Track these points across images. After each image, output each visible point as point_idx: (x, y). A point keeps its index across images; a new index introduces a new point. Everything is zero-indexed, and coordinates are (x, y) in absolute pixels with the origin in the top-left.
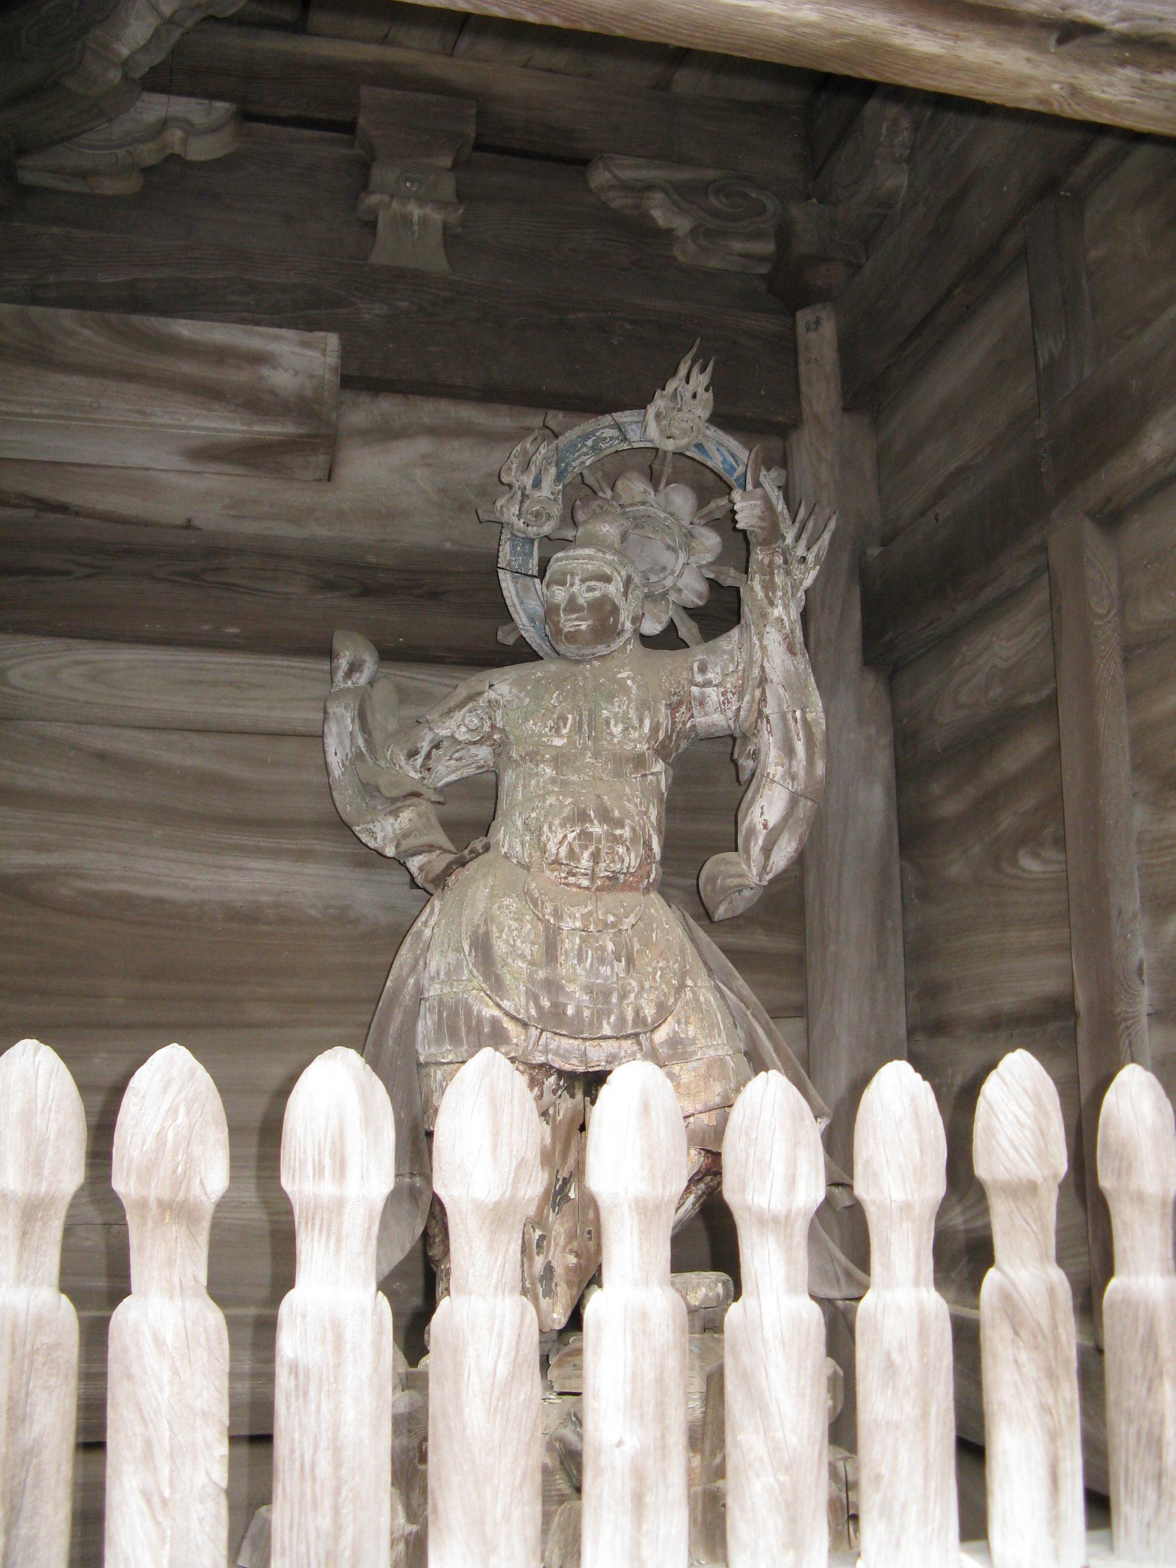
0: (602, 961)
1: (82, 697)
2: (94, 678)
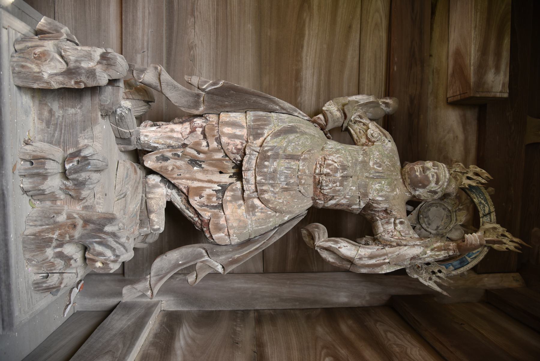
0: (286, 177)
1: (370, 20)
2: (376, 24)
